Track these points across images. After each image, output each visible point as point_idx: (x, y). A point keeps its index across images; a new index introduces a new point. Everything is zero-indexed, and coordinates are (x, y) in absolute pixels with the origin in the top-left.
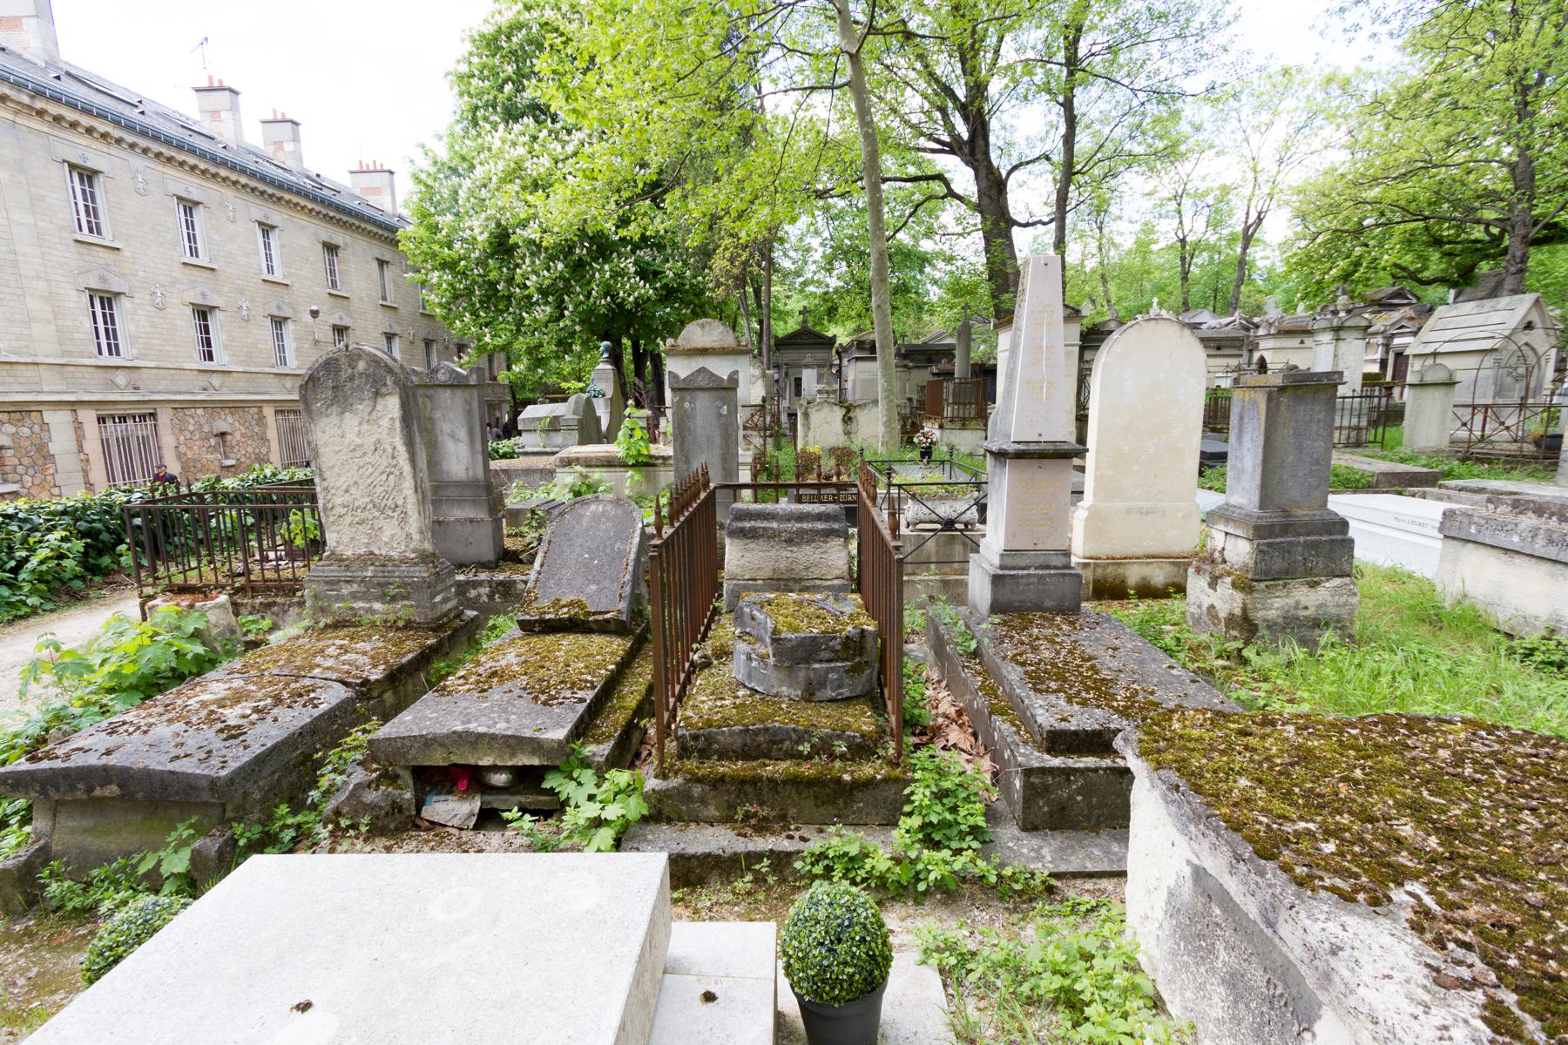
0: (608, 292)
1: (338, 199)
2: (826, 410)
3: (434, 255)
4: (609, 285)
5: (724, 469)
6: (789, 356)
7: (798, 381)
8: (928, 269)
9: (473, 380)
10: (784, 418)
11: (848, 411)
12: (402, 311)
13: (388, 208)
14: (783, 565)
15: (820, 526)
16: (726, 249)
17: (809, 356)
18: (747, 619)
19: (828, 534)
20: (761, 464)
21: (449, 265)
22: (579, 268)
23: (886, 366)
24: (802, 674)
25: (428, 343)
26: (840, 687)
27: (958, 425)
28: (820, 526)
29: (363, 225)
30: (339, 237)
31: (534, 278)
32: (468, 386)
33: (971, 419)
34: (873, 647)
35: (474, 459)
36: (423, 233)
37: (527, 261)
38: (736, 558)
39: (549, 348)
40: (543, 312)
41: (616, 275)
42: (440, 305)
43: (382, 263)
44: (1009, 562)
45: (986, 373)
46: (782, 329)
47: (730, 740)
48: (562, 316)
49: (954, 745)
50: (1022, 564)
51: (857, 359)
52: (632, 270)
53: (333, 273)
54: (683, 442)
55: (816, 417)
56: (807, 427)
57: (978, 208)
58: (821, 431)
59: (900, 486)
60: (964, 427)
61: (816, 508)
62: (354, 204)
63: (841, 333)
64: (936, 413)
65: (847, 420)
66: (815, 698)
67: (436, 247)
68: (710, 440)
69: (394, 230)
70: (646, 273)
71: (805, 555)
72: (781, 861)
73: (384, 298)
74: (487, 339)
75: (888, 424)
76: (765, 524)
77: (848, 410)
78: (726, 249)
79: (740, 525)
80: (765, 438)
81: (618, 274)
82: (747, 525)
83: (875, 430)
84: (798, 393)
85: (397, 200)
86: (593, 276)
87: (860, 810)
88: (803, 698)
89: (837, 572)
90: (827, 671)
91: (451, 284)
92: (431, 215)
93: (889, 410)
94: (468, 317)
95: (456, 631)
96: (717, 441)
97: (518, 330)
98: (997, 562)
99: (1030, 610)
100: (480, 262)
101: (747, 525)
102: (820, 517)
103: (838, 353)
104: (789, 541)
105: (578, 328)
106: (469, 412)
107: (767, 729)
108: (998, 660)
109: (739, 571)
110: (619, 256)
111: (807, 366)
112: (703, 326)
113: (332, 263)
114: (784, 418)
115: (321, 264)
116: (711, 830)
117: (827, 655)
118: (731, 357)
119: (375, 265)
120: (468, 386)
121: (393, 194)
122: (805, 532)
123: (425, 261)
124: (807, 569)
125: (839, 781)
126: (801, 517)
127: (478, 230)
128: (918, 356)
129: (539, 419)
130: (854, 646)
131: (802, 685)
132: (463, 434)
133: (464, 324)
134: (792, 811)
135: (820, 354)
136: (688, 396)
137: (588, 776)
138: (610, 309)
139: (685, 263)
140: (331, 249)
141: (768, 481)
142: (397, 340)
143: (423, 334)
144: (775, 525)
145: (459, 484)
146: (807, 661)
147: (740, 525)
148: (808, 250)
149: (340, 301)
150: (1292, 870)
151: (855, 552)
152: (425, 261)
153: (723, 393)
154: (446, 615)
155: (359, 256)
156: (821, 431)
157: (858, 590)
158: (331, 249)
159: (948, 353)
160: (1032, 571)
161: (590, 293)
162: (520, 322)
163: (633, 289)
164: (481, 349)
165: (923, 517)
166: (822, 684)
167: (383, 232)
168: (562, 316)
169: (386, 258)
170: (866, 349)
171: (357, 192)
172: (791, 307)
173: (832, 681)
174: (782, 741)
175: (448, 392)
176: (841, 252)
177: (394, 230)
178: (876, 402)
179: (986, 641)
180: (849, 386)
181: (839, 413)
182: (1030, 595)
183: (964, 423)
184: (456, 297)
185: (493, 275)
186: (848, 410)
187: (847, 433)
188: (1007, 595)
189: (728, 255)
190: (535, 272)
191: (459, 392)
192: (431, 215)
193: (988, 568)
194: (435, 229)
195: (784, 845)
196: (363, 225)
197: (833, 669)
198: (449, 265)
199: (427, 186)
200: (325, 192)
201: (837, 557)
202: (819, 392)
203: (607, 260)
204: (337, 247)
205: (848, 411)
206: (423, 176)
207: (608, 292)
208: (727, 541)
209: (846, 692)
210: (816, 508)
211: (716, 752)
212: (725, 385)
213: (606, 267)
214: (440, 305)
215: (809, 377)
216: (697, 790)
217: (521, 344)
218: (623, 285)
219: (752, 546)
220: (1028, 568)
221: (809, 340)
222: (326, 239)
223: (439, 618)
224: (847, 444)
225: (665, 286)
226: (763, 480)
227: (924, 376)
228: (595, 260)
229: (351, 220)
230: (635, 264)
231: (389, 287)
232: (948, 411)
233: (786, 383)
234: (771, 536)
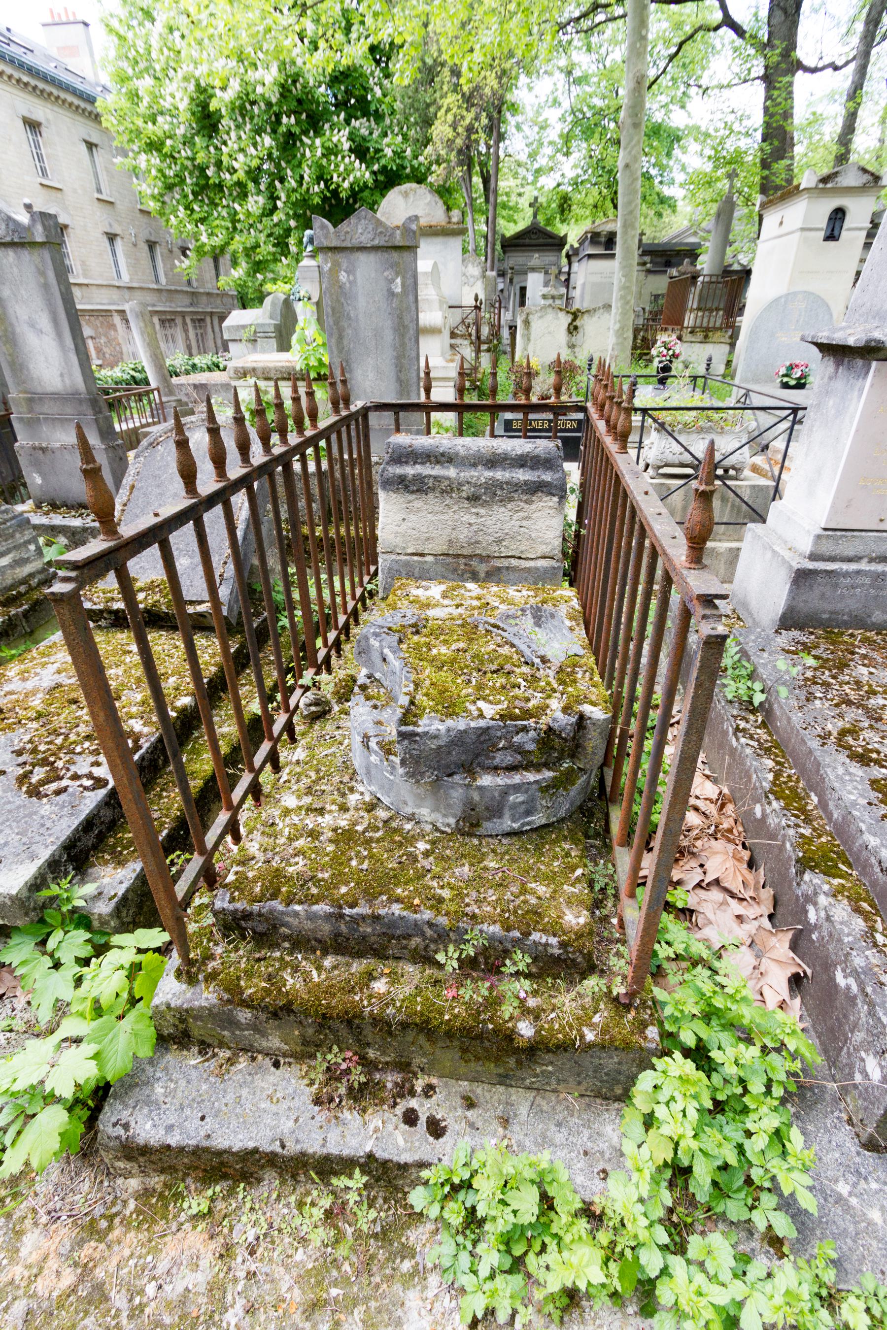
0: (321, 176)
1: (28, 59)
2: (550, 315)
3: (139, 132)
4: (321, 167)
5: (400, 381)
6: (516, 259)
7: (523, 290)
8: (677, 152)
9: (39, 236)
10: (505, 333)
11: (575, 319)
12: (119, 206)
13: (89, 74)
14: (463, 535)
15: (522, 475)
16: (449, 110)
17: (536, 259)
18: (376, 658)
19: (535, 489)
20: (466, 378)
21: (154, 146)
22: (289, 143)
23: (625, 267)
24: (457, 795)
25: (151, 245)
26: (528, 813)
27: (700, 336)
28: (522, 475)
29: (63, 95)
30: (40, 111)
31: (241, 157)
32: (33, 244)
33: (715, 329)
34: (594, 742)
35: (67, 360)
36: (125, 104)
37: (233, 134)
38: (397, 522)
39: (267, 249)
40: (256, 203)
41: (331, 151)
42: (153, 197)
43: (91, 146)
44: (827, 548)
45: (736, 281)
46: (510, 229)
47: (308, 925)
48: (275, 208)
49: (717, 882)
50: (851, 553)
51: (590, 256)
52: (346, 145)
53: (40, 158)
54: (340, 338)
55: (537, 324)
56: (527, 338)
57: (763, 47)
58: (542, 341)
59: (644, 411)
60: (706, 339)
61: (519, 446)
62: (49, 67)
63: (573, 232)
64: (675, 321)
65: (573, 329)
66: (481, 831)
67: (140, 122)
68: (378, 334)
69: (91, 100)
70: (361, 151)
71: (497, 521)
72: (388, 1177)
73: (99, 191)
74: (204, 238)
75: (620, 333)
76: (437, 471)
77: (575, 315)
78: (449, 110)
79: (399, 470)
80: (478, 351)
81: (331, 151)
82: (410, 471)
83: (605, 339)
84: (522, 303)
85: (92, 63)
86: (303, 155)
87: (547, 1075)
88: (459, 831)
89: (543, 549)
90: (506, 791)
91: (160, 171)
92: (129, 79)
93: (624, 314)
94: (182, 212)
95: (36, 606)
96: (389, 336)
97: (235, 228)
98: (806, 545)
99: (847, 625)
100: (188, 142)
101: (410, 471)
102: (522, 462)
103: (568, 256)
104: (474, 499)
105: (293, 223)
106: (46, 286)
107: (376, 918)
108: (814, 744)
109: (399, 541)
110: (332, 128)
111: (533, 270)
112: (406, 195)
113: (37, 146)
114: (505, 333)
115: (26, 146)
116: (274, 1076)
117: (509, 759)
118: (440, 240)
119: (84, 147)
120: (33, 244)
121: (92, 55)
122: (500, 485)
123: (131, 141)
124: (499, 541)
125: (510, 1036)
126: (493, 461)
127: (178, 97)
128: (663, 257)
129: (244, 327)
130: (558, 747)
131: (458, 810)
132: (44, 321)
133: (178, 222)
134: (418, 1061)
135: (548, 258)
136: (341, 258)
137: (72, 943)
138: (325, 199)
139: (405, 138)
140: (33, 126)
141: (475, 404)
142: (119, 240)
143: (144, 235)
144: (451, 472)
145: (56, 397)
146: (469, 769)
147: (399, 470)
148: (543, 127)
149: (53, 193)
150: (290, 134)
151: (572, 516)
152: (131, 141)
153: (395, 255)
154: (24, 581)
155: (63, 130)
156: (542, 341)
157: (572, 577)
158: (33, 126)
159: (692, 253)
160: (864, 566)
161: (302, 177)
162: (233, 218)
163: (348, 172)
164: (200, 251)
165: (671, 458)
166: (495, 811)
167: (82, 103)
168: (275, 208)
169: (94, 140)
170: (604, 243)
171: (54, 53)
172: (523, 191)
173: (514, 807)
174: (408, 937)
175: (11, 253)
176: (585, 125)
177: (91, 100)
178: (608, 307)
179: (783, 692)
180: (576, 294)
181: (565, 320)
182: (849, 603)
183: (706, 334)
184: (170, 187)
185: (201, 157)
186: (575, 315)
187: (572, 346)
188: (814, 601)
189: (450, 118)
190: (242, 150)
191: (25, 254)
192: (129, 79)
193: (787, 555)
194: (134, 97)
195: (397, 1142)
196: (63, 95)
197: (517, 788)
198: (154, 146)
199: (120, 37)
200: (13, 48)
201: (544, 527)
202: (544, 297)
203: (318, 133)
204: (39, 124)
205: (575, 319)
206: (115, 23)
207: (321, 176)
208: (382, 495)
209: (538, 819)
210: (519, 446)
211: (286, 938)
212: (398, 240)
213: (318, 142)
214: (153, 197)
215: (535, 283)
216: (244, 1015)
217: (238, 243)
218: (337, 166)
219: (418, 504)
220: (856, 559)
221: (538, 239)
222: (27, 115)
223: (13, 587)
224: (571, 358)
225: (384, 170)
226: (471, 399)
227: (660, 284)
228: (305, 132)
229: (49, 88)
230: (351, 138)
231: (103, 177)
232: (689, 320)
233: (510, 291)
234: (448, 489)
